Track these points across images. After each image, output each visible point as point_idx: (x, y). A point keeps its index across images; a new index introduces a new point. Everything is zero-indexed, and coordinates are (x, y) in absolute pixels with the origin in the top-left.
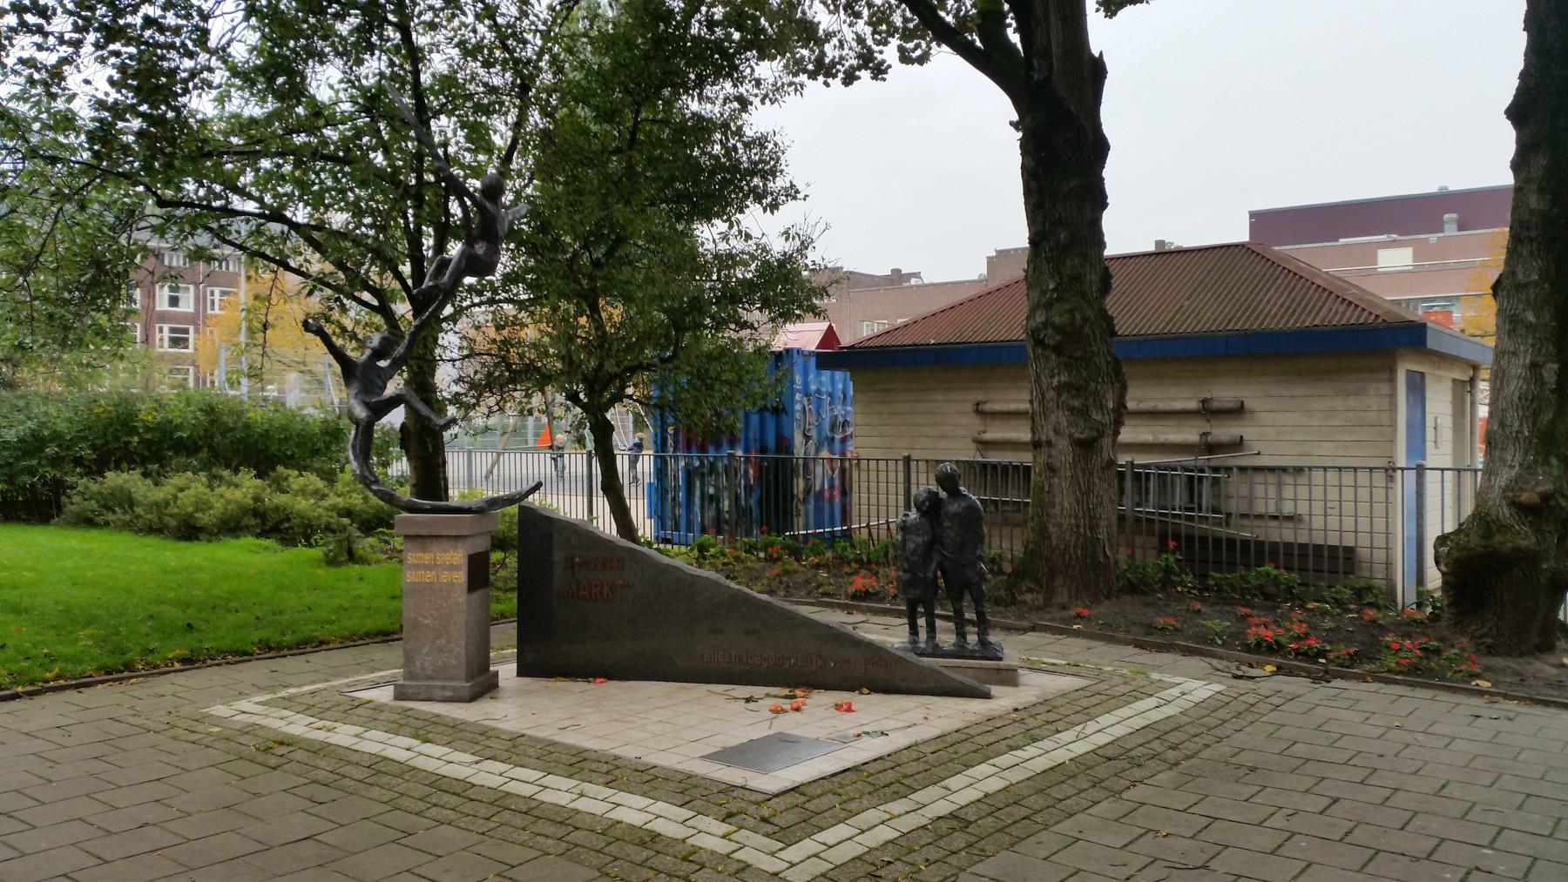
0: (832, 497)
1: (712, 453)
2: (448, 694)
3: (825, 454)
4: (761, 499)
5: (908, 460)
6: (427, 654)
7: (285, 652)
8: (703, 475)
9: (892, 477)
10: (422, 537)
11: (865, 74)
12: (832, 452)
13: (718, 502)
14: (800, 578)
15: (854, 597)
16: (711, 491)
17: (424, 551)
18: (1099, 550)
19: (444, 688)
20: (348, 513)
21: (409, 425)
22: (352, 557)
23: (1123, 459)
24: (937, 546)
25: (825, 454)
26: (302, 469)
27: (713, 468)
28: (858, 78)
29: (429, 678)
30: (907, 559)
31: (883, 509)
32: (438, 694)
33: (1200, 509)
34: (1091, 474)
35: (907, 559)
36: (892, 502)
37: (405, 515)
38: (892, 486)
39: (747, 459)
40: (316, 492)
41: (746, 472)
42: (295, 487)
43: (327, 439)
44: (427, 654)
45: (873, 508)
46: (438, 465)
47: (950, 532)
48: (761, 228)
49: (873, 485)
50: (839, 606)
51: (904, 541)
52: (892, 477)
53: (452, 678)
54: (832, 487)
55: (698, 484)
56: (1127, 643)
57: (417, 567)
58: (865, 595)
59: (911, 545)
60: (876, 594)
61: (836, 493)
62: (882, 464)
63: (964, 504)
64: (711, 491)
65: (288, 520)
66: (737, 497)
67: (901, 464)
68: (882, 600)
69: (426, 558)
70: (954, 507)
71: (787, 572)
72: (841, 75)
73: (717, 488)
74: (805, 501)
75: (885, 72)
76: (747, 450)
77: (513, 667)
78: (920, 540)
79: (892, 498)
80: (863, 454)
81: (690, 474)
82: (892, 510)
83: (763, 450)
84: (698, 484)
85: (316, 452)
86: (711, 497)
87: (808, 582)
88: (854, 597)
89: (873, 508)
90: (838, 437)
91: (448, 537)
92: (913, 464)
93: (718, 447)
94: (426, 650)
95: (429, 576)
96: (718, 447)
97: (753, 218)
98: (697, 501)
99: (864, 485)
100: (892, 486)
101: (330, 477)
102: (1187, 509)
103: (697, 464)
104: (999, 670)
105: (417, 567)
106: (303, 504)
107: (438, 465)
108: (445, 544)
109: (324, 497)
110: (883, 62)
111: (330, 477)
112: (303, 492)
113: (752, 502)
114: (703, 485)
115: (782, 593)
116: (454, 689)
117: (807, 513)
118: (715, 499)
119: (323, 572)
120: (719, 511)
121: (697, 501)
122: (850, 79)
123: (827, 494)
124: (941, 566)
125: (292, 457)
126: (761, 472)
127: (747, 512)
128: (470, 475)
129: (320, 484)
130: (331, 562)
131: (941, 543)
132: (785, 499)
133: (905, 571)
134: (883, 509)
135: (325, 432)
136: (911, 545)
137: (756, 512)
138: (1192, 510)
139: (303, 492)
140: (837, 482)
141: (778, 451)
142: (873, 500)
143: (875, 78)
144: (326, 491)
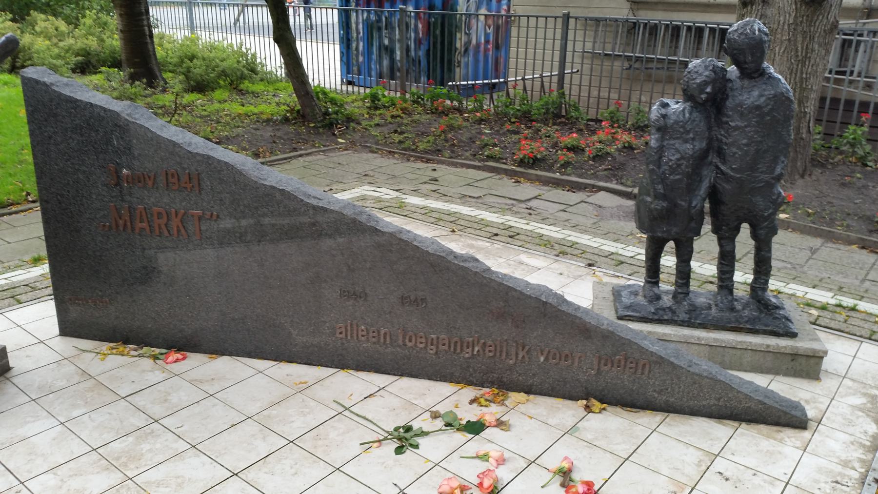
0: (486, 50)
1: (387, 8)
3: (483, 11)
4: (428, 51)
5: (567, 17)
8: (379, 29)
9: (550, 34)
12: (489, 10)
14: (465, 136)
15: (521, 163)
18: (804, 125)
23: (845, 23)
24: (713, 158)
30: (663, 180)
31: (539, 63)
33: (852, 73)
34: (812, 38)
35: (663, 180)
36: (548, 57)
38: (549, 42)
39: (417, 15)
41: (416, 26)
45: (530, 62)
46: (141, 14)
47: (739, 135)
49: (531, 41)
50: (506, 172)
51: (661, 149)
52: (550, 34)
54: (487, 42)
56: (849, 242)
58: (534, 162)
59: (670, 156)
60: (543, 160)
62: (542, 21)
63: (769, 92)
64: (386, 42)
66: (408, 50)
67: (560, 21)
68: (550, 169)
70: (752, 96)
71: (451, 128)
73: (391, 40)
76: (417, 7)
77: (43, 315)
78: (688, 148)
79: (548, 53)
82: (547, 64)
86: (386, 48)
87: (472, 140)
88: (521, 163)
89: (530, 62)
92: (572, 22)
98: (375, 49)
100: (549, 42)
102: (837, 73)
103: (373, 17)
104: (795, 356)
107: (141, 14)
113: (422, 53)
115: (447, 153)
117: (467, 65)
118: (390, 51)
120: (392, 60)
121: (375, 49)
123: (482, 47)
124: (714, 195)
126: (428, 27)
127: (416, 62)
128: (192, 23)
131: (720, 153)
132: (450, 51)
133: (657, 197)
134: (539, 63)
136: (670, 156)
137: (424, 63)
138: (843, 73)
142: (539, 56)
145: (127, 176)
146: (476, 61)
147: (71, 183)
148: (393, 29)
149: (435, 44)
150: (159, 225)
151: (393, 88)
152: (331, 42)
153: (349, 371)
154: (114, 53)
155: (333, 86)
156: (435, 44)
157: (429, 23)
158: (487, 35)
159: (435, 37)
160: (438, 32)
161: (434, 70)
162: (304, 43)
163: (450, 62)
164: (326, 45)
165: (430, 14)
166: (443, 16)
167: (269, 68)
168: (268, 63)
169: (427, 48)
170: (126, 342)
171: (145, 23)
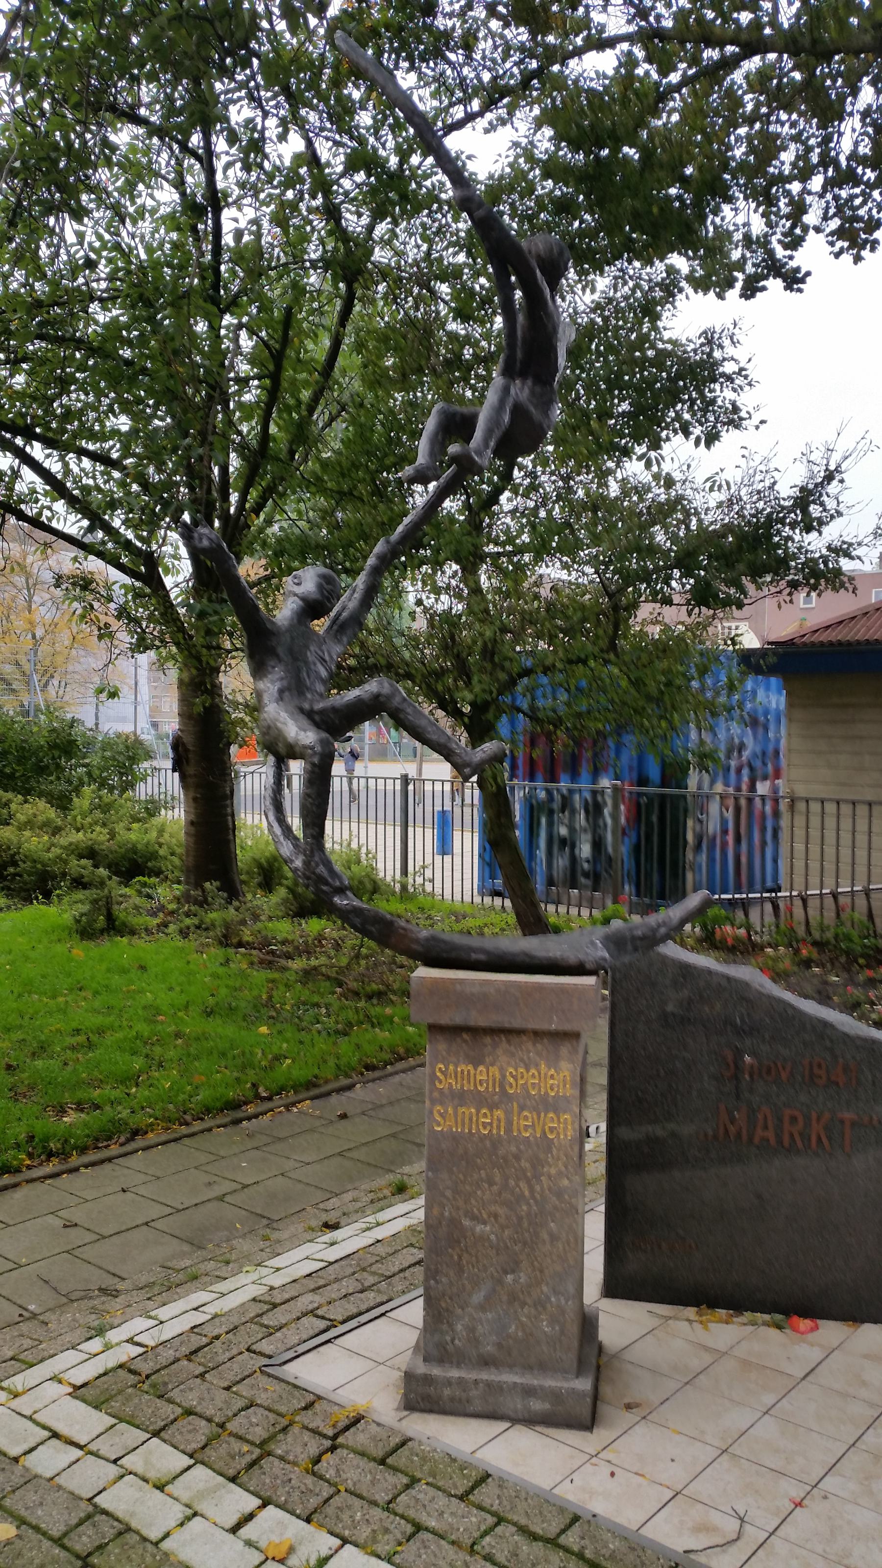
0: (724, 845)
1: (564, 784)
2: (537, 1406)
3: (719, 788)
6: (482, 1308)
7: (75, 1160)
8: (551, 813)
10: (476, 1032)
11: (775, 285)
12: (727, 784)
13: (573, 846)
16: (563, 831)
17: (476, 1062)
19: (529, 1392)
20: (91, 853)
21: (188, 739)
22: (114, 927)
25: (719, 788)
26: (26, 792)
27: (566, 803)
28: (764, 289)
29: (486, 1362)
32: (516, 1404)
37: (423, 972)
40: (46, 824)
42: (21, 817)
43: (56, 753)
44: (482, 1308)
48: (701, 472)
53: (543, 1367)
54: (725, 832)
55: (543, 821)
57: (460, 1098)
61: (730, 838)
65: (15, 864)
69: (483, 1076)
72: (739, 285)
73: (572, 829)
74: (698, 847)
75: (802, 281)
80: (801, 790)
81: (533, 810)
83: (642, 781)
84: (543, 821)
85: (41, 770)
86: (563, 842)
90: (733, 763)
91: (538, 1035)
93: (575, 776)
94: (478, 1298)
95: (486, 1122)
96: (575, 776)
97: (678, 452)
99: (800, 833)
101: (62, 803)
103: (542, 795)
105: (460, 1098)
106: (34, 843)
108: (530, 1049)
109: (57, 831)
110: (797, 270)
111: (62, 803)
112: (29, 824)
113: (625, 850)
114: (550, 824)
116: (556, 1396)
118: (568, 844)
119: (80, 951)
122: (751, 290)
125: (11, 776)
129: (52, 813)
130: (86, 932)
135: (53, 746)
139: (29, 824)
140: (731, 826)
141: (664, 784)
143: (789, 287)
144: (59, 822)
145: (752, 1066)
146: (711, 860)
147: (662, 1073)
148: (573, 812)
149: (648, 837)
150: (792, 1135)
151: (574, 901)
152: (372, 819)
153: (538, 1428)
154: (135, 853)
155: (467, 898)
156: (648, 837)
157: (638, 805)
158: (724, 822)
159: (649, 824)
160: (654, 819)
161: (649, 875)
162: (337, 824)
163: (675, 864)
164: (381, 828)
165: (639, 794)
166: (663, 797)
167: (382, 875)
168: (380, 866)
169: (634, 839)
170: (713, 1303)
171: (229, 810)
